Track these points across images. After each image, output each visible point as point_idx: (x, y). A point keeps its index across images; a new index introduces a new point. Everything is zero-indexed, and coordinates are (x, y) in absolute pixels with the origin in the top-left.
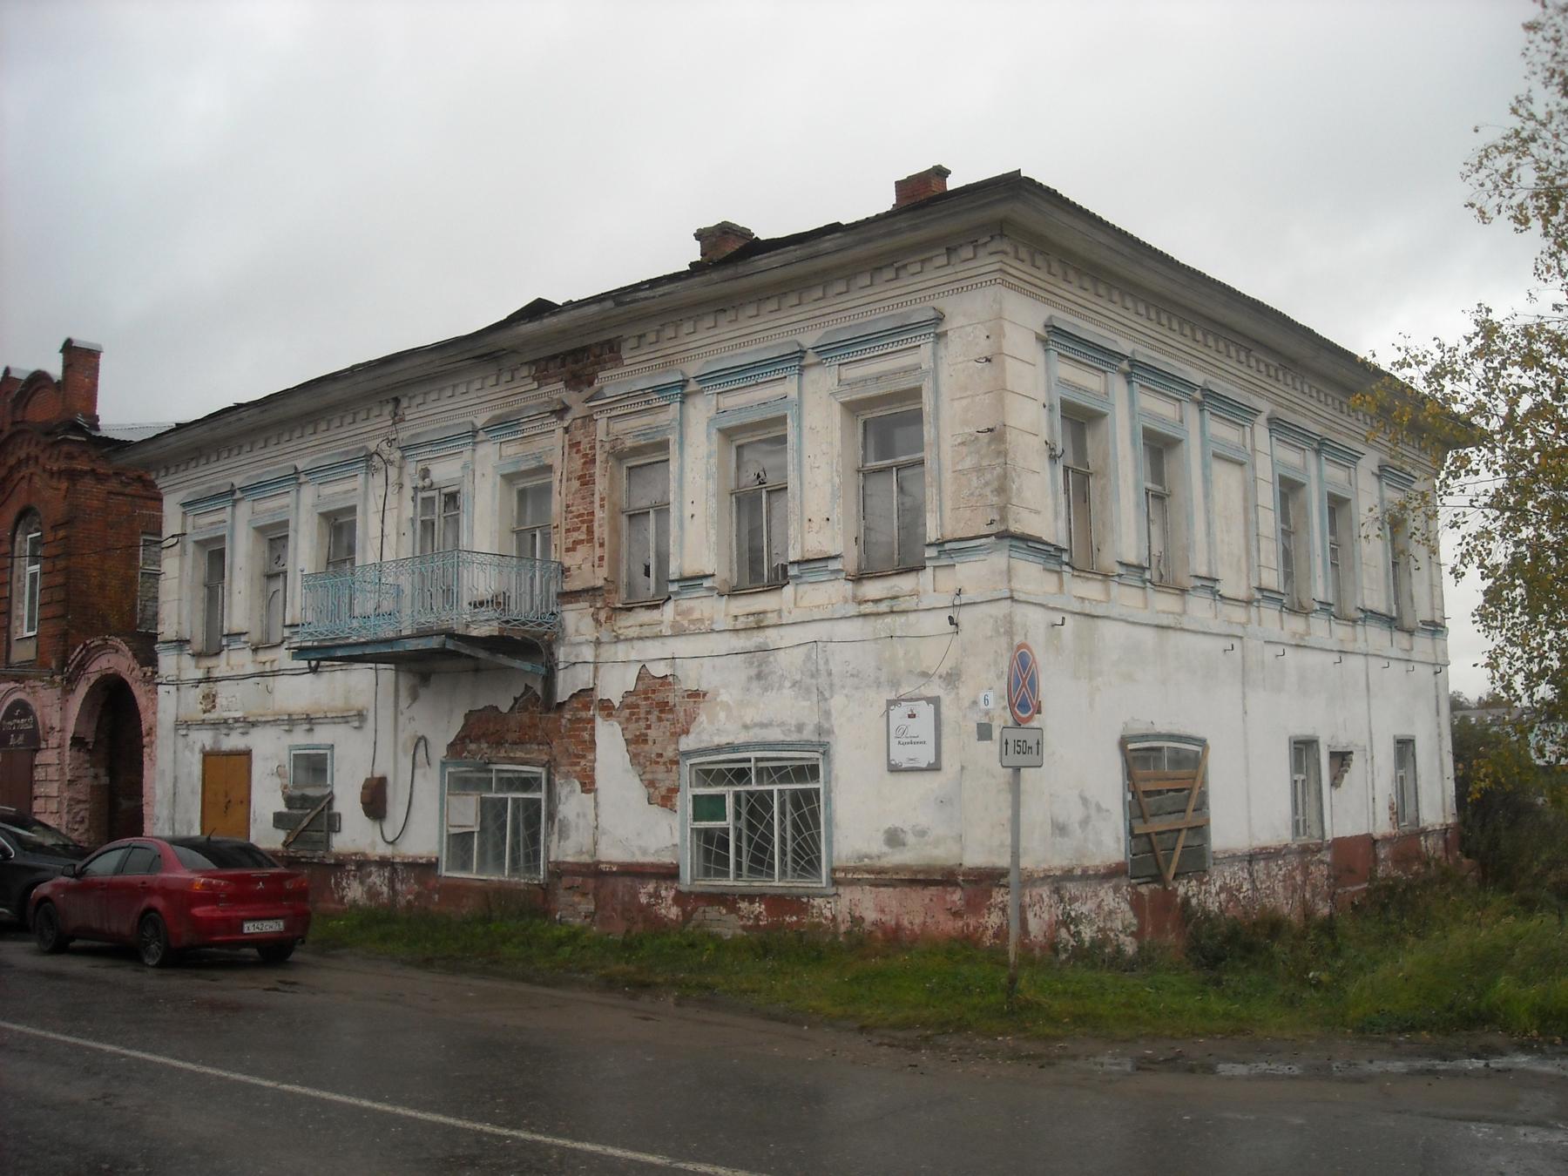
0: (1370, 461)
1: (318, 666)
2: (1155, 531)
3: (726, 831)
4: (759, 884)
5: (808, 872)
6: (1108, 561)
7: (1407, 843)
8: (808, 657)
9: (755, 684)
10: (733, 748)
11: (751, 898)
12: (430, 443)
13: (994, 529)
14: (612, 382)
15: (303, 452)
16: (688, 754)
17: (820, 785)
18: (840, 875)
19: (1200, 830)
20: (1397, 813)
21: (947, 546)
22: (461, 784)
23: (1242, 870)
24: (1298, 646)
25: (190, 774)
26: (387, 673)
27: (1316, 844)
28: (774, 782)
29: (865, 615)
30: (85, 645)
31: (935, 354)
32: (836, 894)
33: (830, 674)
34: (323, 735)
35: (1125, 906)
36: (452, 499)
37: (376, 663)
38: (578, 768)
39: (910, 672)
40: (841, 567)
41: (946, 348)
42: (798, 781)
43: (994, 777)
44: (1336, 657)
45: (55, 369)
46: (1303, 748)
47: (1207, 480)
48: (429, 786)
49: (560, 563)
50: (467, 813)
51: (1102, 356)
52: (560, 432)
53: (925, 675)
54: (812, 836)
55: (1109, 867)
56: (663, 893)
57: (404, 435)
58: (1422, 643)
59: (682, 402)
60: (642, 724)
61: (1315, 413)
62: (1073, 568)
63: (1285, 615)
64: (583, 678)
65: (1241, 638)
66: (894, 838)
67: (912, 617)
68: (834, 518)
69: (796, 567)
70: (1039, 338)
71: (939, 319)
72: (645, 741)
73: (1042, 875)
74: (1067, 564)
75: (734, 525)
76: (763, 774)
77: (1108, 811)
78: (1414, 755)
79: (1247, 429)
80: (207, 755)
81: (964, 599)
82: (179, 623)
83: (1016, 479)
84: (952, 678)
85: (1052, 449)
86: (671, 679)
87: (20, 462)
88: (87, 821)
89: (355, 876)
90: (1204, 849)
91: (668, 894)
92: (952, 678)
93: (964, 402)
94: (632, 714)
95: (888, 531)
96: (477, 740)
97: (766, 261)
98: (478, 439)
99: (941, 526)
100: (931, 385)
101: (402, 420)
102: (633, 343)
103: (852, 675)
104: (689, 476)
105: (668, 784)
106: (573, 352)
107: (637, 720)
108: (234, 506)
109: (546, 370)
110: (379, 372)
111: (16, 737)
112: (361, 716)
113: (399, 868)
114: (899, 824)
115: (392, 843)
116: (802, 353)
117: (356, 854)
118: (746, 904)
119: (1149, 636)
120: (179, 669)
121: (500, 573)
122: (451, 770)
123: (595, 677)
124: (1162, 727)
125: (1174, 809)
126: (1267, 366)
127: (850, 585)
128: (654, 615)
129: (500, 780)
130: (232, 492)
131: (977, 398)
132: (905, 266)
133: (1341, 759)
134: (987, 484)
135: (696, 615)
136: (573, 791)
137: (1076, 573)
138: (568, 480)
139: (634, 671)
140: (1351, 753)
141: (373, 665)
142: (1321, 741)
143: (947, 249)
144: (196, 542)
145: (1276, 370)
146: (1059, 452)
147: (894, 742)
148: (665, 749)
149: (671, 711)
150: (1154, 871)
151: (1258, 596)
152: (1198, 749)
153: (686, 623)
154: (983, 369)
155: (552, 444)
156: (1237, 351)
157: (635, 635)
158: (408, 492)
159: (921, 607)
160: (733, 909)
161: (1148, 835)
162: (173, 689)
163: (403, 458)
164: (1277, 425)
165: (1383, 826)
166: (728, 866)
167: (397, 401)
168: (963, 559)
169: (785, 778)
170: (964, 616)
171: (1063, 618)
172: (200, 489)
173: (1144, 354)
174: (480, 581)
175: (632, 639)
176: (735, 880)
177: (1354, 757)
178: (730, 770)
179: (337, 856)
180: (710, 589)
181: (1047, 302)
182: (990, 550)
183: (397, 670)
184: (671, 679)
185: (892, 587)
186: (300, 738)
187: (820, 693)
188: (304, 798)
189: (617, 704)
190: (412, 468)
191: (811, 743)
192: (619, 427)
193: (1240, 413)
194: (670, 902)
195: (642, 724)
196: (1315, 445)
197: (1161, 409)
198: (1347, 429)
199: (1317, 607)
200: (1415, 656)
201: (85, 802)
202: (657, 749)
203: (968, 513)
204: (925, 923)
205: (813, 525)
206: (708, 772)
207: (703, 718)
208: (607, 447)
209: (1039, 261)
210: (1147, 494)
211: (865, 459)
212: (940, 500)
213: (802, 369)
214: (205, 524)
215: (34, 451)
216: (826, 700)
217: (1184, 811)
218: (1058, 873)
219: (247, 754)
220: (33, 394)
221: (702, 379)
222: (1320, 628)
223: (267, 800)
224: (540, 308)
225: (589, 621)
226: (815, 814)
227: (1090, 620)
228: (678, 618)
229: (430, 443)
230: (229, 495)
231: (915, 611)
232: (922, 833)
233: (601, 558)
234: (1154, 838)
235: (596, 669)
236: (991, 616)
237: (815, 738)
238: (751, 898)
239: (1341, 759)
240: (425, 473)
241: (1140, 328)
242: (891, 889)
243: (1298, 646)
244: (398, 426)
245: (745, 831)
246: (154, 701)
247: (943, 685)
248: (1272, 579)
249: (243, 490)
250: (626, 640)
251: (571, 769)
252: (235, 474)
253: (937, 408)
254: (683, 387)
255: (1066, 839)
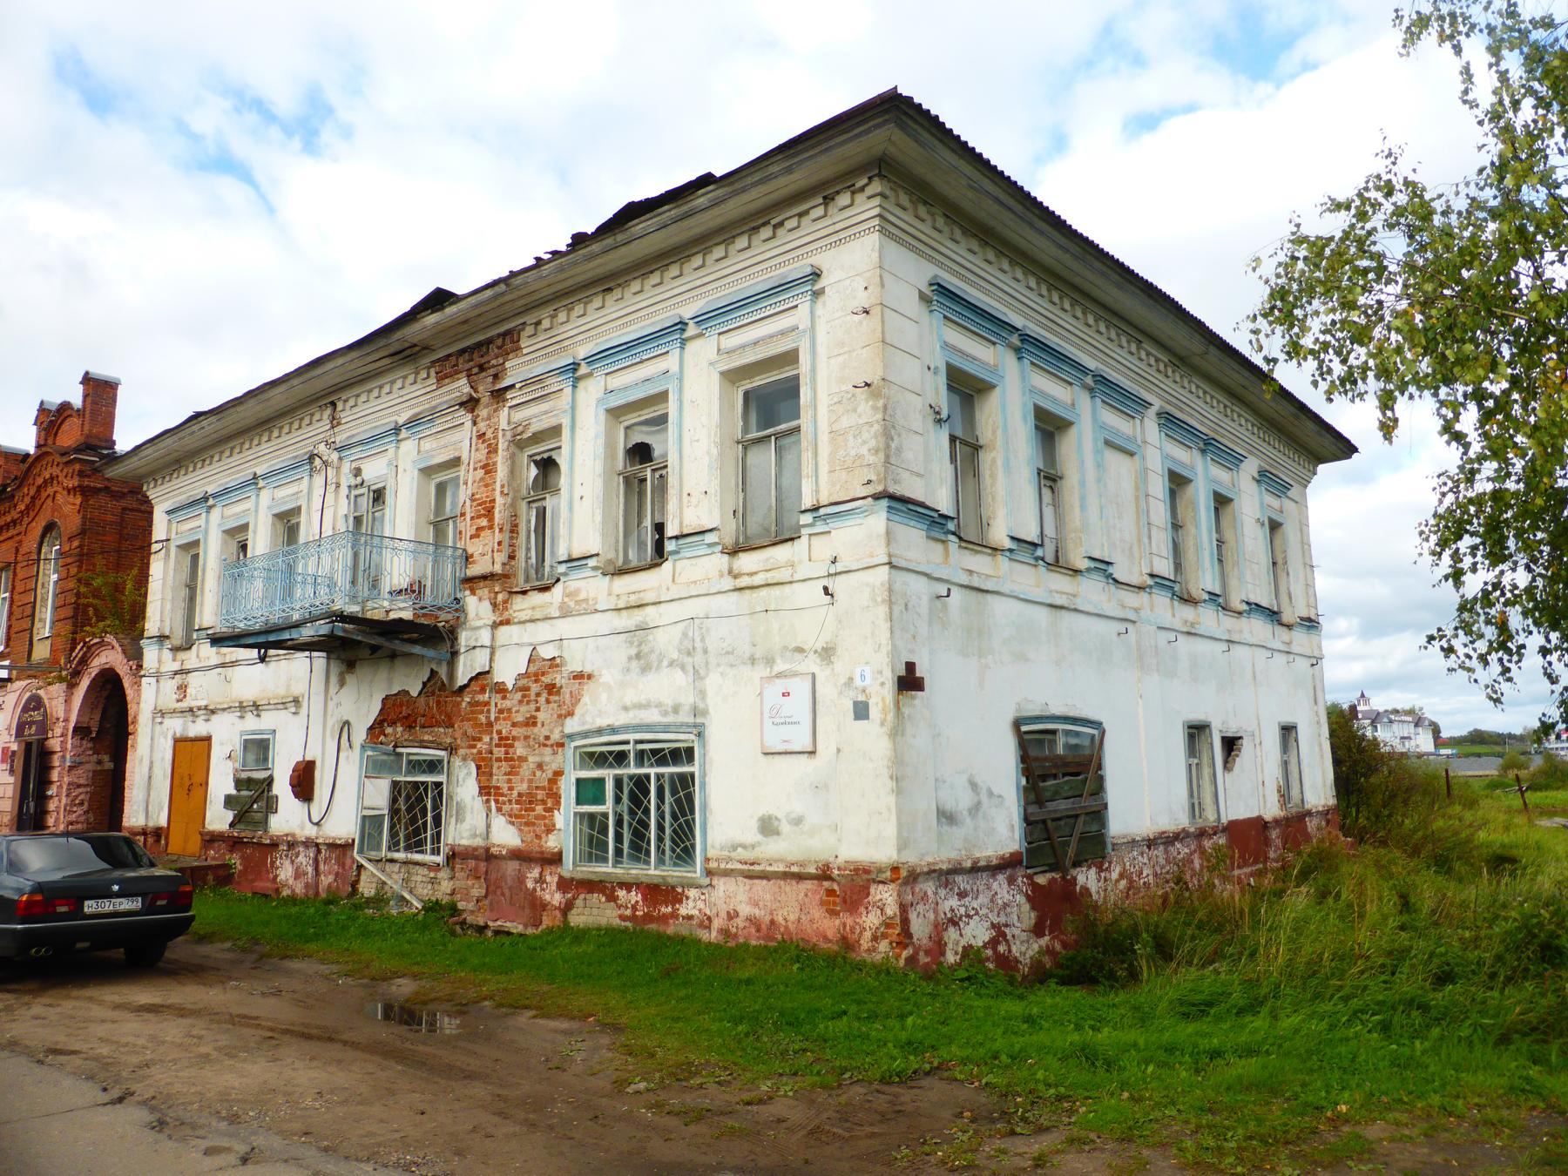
0: (1251, 466)
1: (265, 655)
2: (1048, 512)
3: (605, 815)
4: (634, 871)
5: (685, 862)
6: (999, 535)
7: (1294, 824)
8: (685, 635)
9: (635, 664)
10: (613, 730)
11: (627, 886)
12: (361, 443)
13: (870, 490)
14: (516, 370)
15: (264, 455)
16: (571, 737)
17: (695, 768)
18: (713, 865)
19: (1099, 815)
20: (1284, 796)
21: (822, 512)
22: (374, 769)
23: (1142, 854)
24: (1189, 633)
25: (163, 759)
26: (320, 658)
27: (1213, 828)
28: (652, 766)
29: (741, 589)
30: (85, 643)
31: (812, 313)
32: (711, 885)
33: (705, 651)
34: (268, 720)
35: (1020, 899)
36: (378, 496)
37: (311, 651)
38: (475, 751)
39: (785, 648)
40: (717, 540)
41: (824, 305)
42: (675, 764)
43: (871, 760)
44: (1224, 646)
45: (77, 400)
46: (1196, 732)
47: (1099, 466)
48: (352, 765)
49: (465, 550)
50: (379, 794)
51: (991, 325)
52: (469, 424)
53: (800, 650)
54: (687, 822)
55: (1002, 858)
56: (548, 878)
57: (340, 439)
58: (1300, 639)
59: (574, 387)
60: (533, 706)
61: (1204, 411)
62: (960, 539)
63: (1176, 603)
64: (479, 661)
65: (1134, 622)
66: (768, 827)
67: (787, 588)
68: (711, 491)
69: (674, 541)
70: (923, 297)
71: (816, 275)
72: (535, 724)
73: (925, 869)
74: (954, 533)
75: (622, 506)
76: (641, 757)
77: (1000, 796)
78: (1296, 741)
79: (1138, 421)
80: (177, 741)
81: (839, 567)
82: (162, 621)
83: (896, 437)
84: (827, 653)
85: (938, 413)
86: (558, 661)
87: (45, 481)
88: (86, 804)
89: (287, 856)
90: (1102, 835)
91: (552, 880)
92: (827, 653)
93: (841, 359)
94: (524, 696)
95: (765, 500)
96: (393, 724)
97: (641, 226)
98: (400, 437)
99: (817, 492)
100: (808, 345)
101: (339, 424)
102: (529, 330)
103: (728, 653)
104: (579, 458)
105: (554, 767)
106: (479, 345)
107: (528, 702)
108: (208, 512)
109: (456, 365)
110: (309, 375)
111: (30, 728)
112: (296, 701)
113: (323, 848)
114: (773, 811)
115: (317, 824)
116: (682, 325)
117: (287, 835)
118: (624, 892)
119: (1042, 614)
120: (159, 661)
121: (415, 559)
122: (370, 753)
123: (491, 660)
124: (1057, 709)
125: (1070, 794)
126: (1157, 360)
127: (726, 557)
128: (546, 596)
129: (409, 762)
130: (205, 499)
131: (855, 354)
132: (781, 224)
133: (1231, 744)
134: (864, 442)
135: (582, 596)
136: (469, 774)
137: (964, 544)
138: (475, 469)
139: (526, 652)
140: (1240, 738)
141: (307, 653)
142: (1213, 726)
143: (825, 198)
144: (178, 546)
145: (1166, 366)
146: (944, 415)
147: (768, 722)
148: (551, 731)
149: (558, 693)
150: (1051, 861)
151: (1150, 582)
152: (1095, 732)
153: (572, 604)
154: (860, 323)
155: (460, 439)
156: (1128, 342)
157: (528, 618)
158: (344, 491)
159: (796, 578)
160: (612, 898)
161: (1044, 822)
162: (153, 680)
163: (340, 459)
164: (1169, 421)
165: (1271, 809)
166: (607, 852)
167: (333, 404)
168: (839, 524)
169: (662, 761)
170: (836, 585)
171: (949, 590)
172: (182, 498)
173: (1034, 330)
174: (398, 569)
175: (524, 622)
176: (614, 866)
177: (1245, 742)
178: (610, 753)
179: (271, 838)
180: (595, 568)
181: (930, 259)
182: (867, 512)
183: (328, 658)
184: (558, 661)
185: (767, 560)
186: (251, 723)
187: (696, 671)
188: (250, 781)
189: (510, 687)
190: (346, 467)
191: (688, 725)
192: (518, 416)
193: (1130, 403)
194: (554, 888)
195: (533, 706)
196: (1202, 445)
197: (1058, 393)
198: (1236, 429)
199: (1206, 597)
200: (1295, 648)
201: (85, 786)
202: (545, 732)
203: (844, 476)
204: (799, 920)
205: (692, 499)
206: (591, 755)
207: (586, 699)
208: (509, 435)
209: (922, 210)
210: (1039, 474)
211: (746, 430)
212: (816, 464)
213: (684, 342)
214: (185, 530)
215: (56, 471)
216: (702, 679)
217: (1081, 796)
218: (944, 867)
219: (208, 739)
220: (62, 423)
221: (591, 359)
222: (1208, 618)
223: (221, 783)
224: (439, 299)
225: (486, 605)
226: (690, 799)
227: (980, 595)
228: (566, 599)
229: (361, 443)
230: (204, 501)
231: (791, 582)
232: (798, 821)
233: (500, 543)
234: (1050, 824)
235: (492, 654)
236: (867, 585)
237: (691, 720)
238: (627, 886)
239: (1231, 744)
240: (357, 472)
241: (1029, 302)
242: (765, 882)
243: (1189, 633)
244: (336, 430)
245: (626, 817)
246: (139, 691)
247: (818, 660)
248: (1165, 568)
249: (214, 496)
250: (520, 623)
251: (468, 751)
252: (209, 483)
253: (814, 370)
254: (575, 370)
255: (954, 828)
